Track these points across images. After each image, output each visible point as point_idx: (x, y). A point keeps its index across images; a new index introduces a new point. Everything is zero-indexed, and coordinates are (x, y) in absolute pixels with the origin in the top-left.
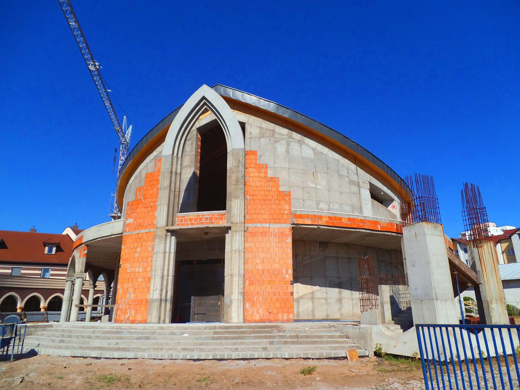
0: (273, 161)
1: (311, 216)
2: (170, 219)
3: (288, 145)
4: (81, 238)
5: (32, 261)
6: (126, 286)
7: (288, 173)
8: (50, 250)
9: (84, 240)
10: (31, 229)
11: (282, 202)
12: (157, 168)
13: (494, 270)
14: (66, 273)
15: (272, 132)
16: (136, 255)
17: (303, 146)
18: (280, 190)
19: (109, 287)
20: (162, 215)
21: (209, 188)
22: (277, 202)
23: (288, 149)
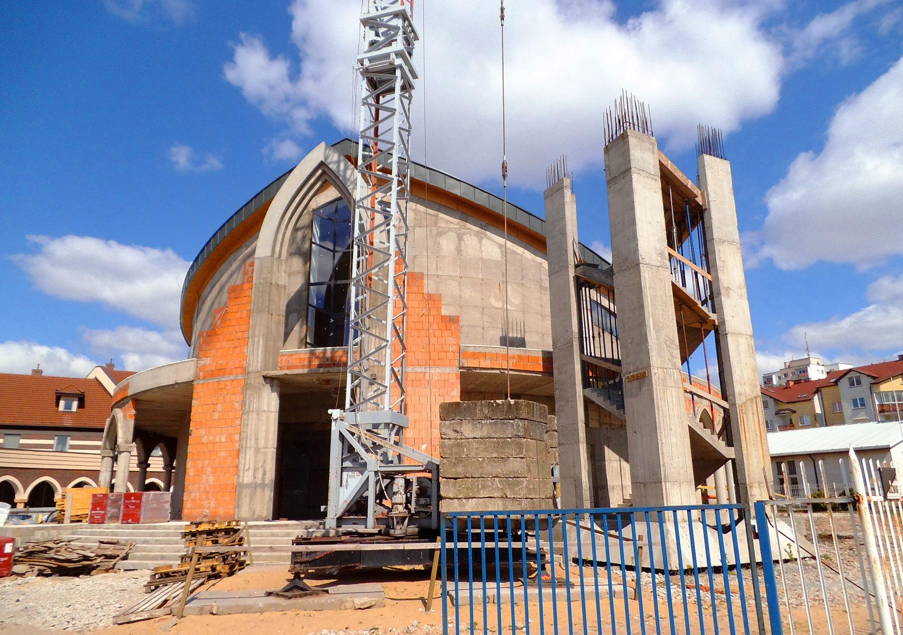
0: (435, 266)
1: (491, 354)
2: (271, 352)
3: (460, 238)
4: (126, 388)
5: (39, 424)
6: (200, 463)
7: (459, 284)
8: (68, 406)
9: (131, 392)
10: (34, 371)
11: (446, 333)
12: (246, 277)
13: (759, 439)
14: (99, 443)
15: (433, 218)
16: (216, 416)
17: (484, 241)
18: (443, 314)
19: (169, 466)
20: (255, 352)
21: (327, 315)
22: (438, 333)
23: (459, 245)
